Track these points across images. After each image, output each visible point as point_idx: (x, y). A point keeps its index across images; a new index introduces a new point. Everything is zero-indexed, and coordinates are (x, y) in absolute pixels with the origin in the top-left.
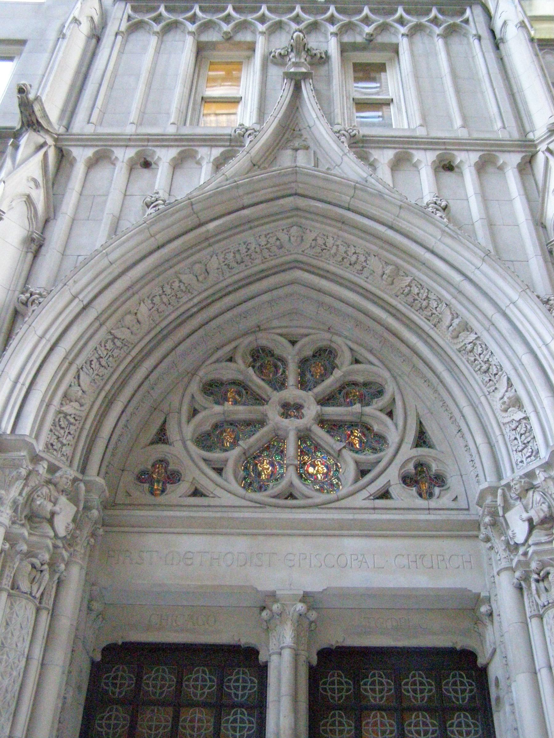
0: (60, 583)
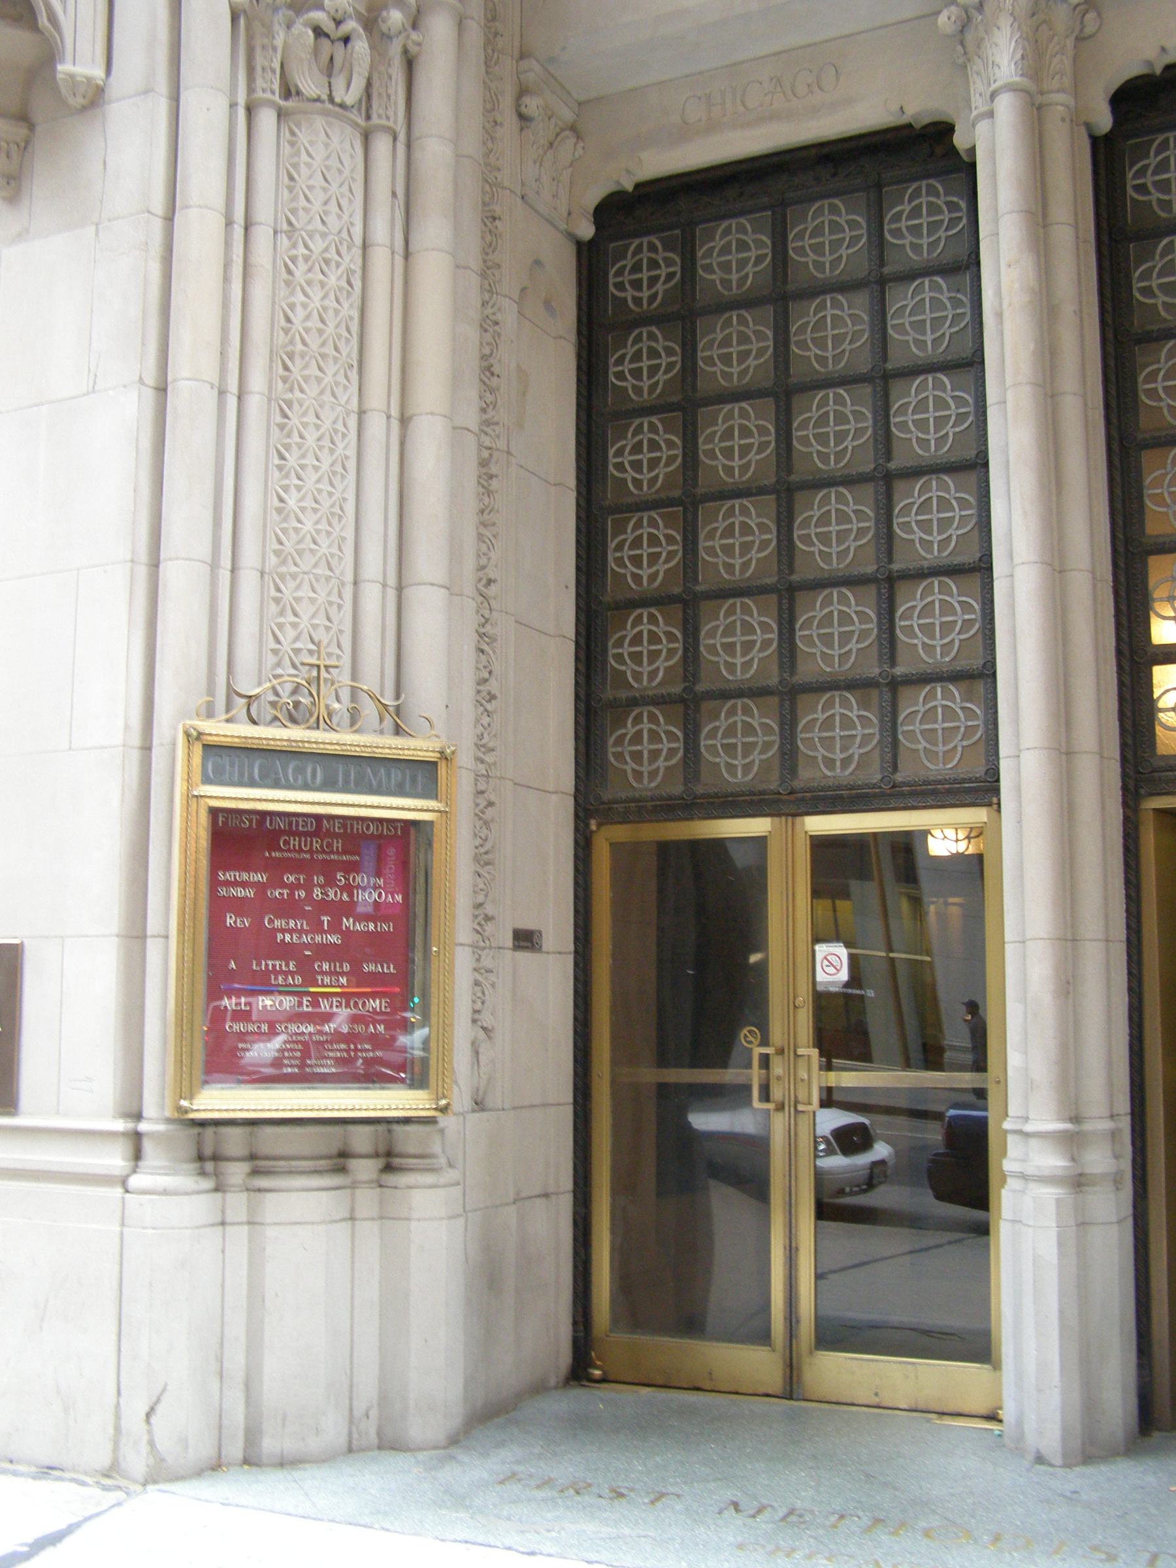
0: (410, 64)
